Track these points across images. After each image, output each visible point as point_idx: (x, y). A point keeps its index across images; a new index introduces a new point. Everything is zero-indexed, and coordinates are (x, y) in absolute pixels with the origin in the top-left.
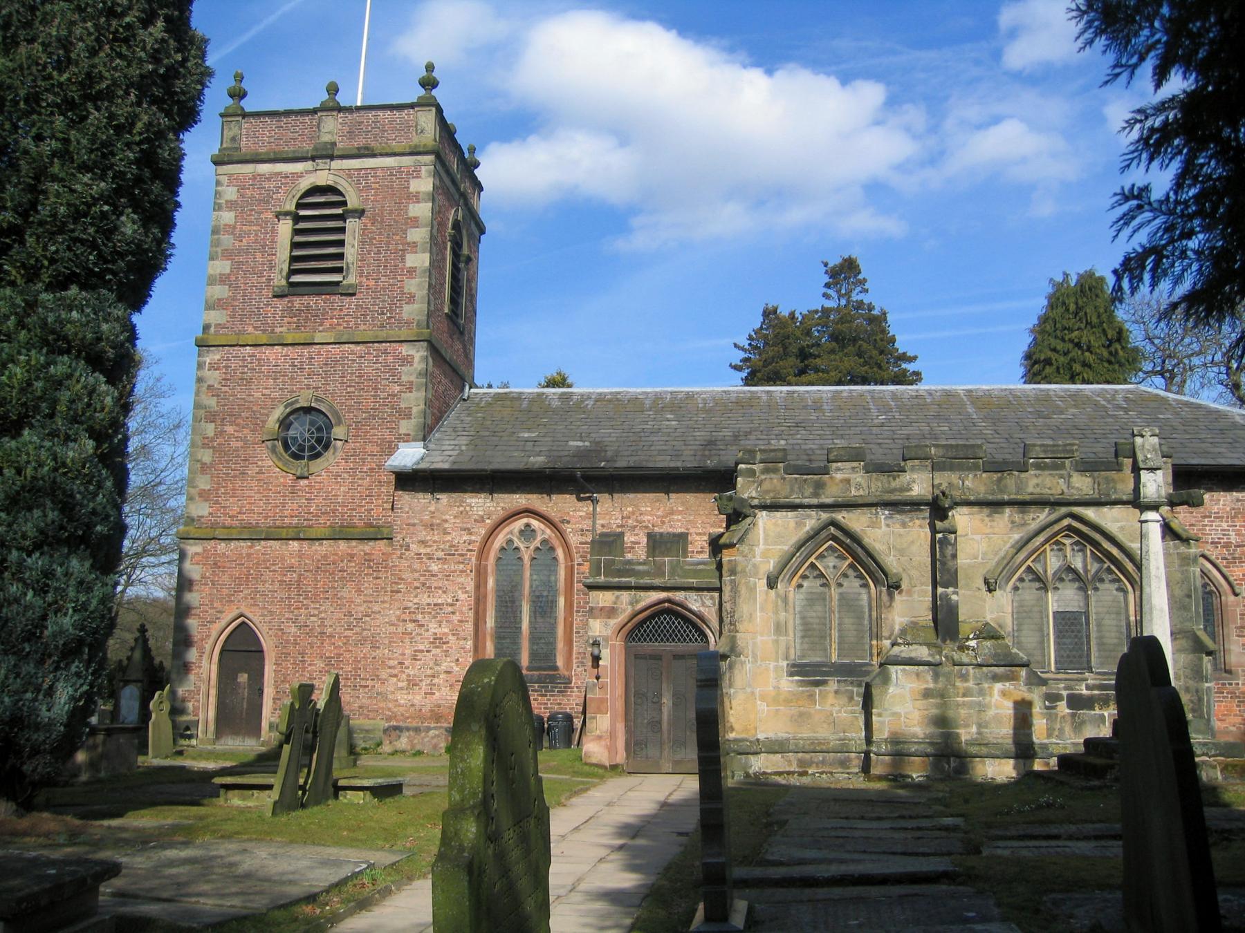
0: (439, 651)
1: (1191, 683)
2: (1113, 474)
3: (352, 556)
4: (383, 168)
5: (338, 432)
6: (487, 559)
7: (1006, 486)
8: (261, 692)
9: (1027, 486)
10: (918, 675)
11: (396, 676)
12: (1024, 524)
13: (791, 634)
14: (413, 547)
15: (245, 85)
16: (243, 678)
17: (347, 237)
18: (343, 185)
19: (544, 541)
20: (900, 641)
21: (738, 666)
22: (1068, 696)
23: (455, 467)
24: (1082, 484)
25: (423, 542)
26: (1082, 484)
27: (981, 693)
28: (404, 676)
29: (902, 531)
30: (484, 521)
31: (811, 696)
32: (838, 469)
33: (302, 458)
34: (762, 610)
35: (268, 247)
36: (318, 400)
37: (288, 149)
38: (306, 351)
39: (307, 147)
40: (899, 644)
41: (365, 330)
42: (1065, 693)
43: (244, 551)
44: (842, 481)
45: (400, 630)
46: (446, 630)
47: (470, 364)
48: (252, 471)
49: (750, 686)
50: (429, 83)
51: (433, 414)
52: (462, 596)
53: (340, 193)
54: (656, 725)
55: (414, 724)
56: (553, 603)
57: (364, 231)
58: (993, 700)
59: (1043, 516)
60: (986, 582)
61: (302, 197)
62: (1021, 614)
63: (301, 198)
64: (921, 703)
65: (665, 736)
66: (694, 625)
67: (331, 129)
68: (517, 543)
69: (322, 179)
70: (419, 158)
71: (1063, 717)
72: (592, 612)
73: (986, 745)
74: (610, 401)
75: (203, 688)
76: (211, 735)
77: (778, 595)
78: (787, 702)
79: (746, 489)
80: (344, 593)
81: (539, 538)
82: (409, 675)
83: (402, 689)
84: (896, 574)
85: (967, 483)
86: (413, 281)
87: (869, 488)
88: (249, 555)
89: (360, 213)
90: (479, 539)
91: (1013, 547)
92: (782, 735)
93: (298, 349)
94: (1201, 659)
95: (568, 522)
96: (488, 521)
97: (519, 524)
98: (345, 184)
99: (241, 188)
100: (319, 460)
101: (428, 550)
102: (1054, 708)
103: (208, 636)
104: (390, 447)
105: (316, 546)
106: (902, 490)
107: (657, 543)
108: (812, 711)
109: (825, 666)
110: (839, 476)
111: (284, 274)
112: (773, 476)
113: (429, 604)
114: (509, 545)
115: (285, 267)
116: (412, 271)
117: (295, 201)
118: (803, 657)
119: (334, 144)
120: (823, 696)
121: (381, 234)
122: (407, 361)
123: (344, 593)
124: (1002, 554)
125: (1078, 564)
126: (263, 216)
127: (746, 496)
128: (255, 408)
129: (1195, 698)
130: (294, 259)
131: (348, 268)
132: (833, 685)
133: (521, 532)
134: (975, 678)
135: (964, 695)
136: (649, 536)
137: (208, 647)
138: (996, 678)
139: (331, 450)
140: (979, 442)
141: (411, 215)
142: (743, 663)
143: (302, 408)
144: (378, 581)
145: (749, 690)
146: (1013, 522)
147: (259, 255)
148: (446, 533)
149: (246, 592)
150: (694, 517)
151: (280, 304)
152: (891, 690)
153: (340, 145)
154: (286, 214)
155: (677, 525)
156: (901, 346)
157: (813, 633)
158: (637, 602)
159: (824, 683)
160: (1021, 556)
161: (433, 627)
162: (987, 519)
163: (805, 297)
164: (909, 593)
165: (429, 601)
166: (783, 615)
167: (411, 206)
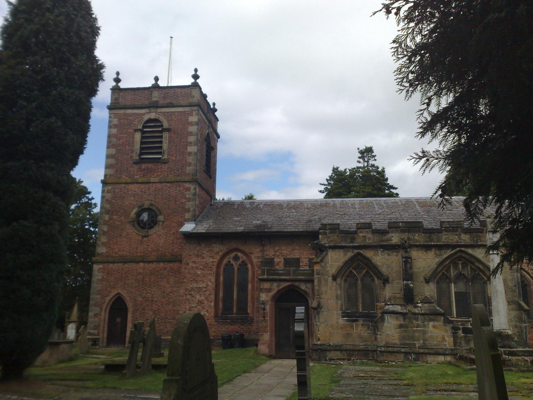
0: (200, 307)
1: (518, 324)
2: (480, 234)
3: (165, 268)
4: (178, 112)
5: (161, 218)
12: (441, 255)
14: (190, 264)
15: (120, 77)
17: (164, 140)
18: (162, 118)
19: (243, 262)
21: (321, 313)
23: (207, 232)
24: (465, 238)
26: (465, 238)
27: (424, 326)
29: (388, 257)
31: (352, 326)
32: (361, 232)
33: (145, 228)
36: (151, 205)
37: (138, 104)
38: (147, 186)
39: (146, 102)
40: (388, 305)
41: (171, 178)
42: (461, 327)
44: (363, 237)
45: (184, 298)
48: (124, 234)
49: (326, 321)
50: (196, 77)
51: (199, 211)
52: (210, 284)
57: (170, 137)
58: (430, 329)
59: (449, 252)
60: (425, 279)
61: (144, 124)
62: (440, 292)
64: (398, 330)
67: (156, 96)
68: (232, 262)
69: (153, 116)
70: (192, 108)
71: (461, 337)
72: (261, 290)
73: (427, 348)
74: (270, 205)
75: (102, 324)
77: (337, 284)
78: (342, 328)
79: (323, 240)
81: (241, 260)
86: (190, 158)
89: (168, 130)
91: (436, 264)
92: (340, 343)
94: (521, 314)
95: (253, 253)
96: (221, 253)
97: (233, 255)
99: (120, 119)
100: (152, 229)
101: (196, 265)
105: (151, 265)
107: (288, 262)
111: (138, 154)
113: (196, 288)
114: (229, 264)
115: (138, 151)
116: (190, 154)
117: (142, 125)
119: (157, 102)
122: (188, 189)
126: (129, 131)
127: (323, 243)
128: (126, 208)
129: (520, 331)
130: (142, 149)
131: (164, 153)
132: (361, 322)
135: (417, 327)
136: (285, 259)
137: (104, 307)
138: (431, 320)
139: (157, 225)
140: (421, 220)
142: (323, 312)
143: (145, 208)
145: (326, 323)
146: (436, 254)
147: (127, 147)
148: (203, 258)
150: (303, 254)
151: (136, 167)
152: (385, 324)
153: (161, 102)
155: (296, 254)
156: (390, 182)
157: (350, 299)
158: (280, 286)
161: (198, 297)
162: (424, 252)
163: (349, 163)
165: (197, 286)
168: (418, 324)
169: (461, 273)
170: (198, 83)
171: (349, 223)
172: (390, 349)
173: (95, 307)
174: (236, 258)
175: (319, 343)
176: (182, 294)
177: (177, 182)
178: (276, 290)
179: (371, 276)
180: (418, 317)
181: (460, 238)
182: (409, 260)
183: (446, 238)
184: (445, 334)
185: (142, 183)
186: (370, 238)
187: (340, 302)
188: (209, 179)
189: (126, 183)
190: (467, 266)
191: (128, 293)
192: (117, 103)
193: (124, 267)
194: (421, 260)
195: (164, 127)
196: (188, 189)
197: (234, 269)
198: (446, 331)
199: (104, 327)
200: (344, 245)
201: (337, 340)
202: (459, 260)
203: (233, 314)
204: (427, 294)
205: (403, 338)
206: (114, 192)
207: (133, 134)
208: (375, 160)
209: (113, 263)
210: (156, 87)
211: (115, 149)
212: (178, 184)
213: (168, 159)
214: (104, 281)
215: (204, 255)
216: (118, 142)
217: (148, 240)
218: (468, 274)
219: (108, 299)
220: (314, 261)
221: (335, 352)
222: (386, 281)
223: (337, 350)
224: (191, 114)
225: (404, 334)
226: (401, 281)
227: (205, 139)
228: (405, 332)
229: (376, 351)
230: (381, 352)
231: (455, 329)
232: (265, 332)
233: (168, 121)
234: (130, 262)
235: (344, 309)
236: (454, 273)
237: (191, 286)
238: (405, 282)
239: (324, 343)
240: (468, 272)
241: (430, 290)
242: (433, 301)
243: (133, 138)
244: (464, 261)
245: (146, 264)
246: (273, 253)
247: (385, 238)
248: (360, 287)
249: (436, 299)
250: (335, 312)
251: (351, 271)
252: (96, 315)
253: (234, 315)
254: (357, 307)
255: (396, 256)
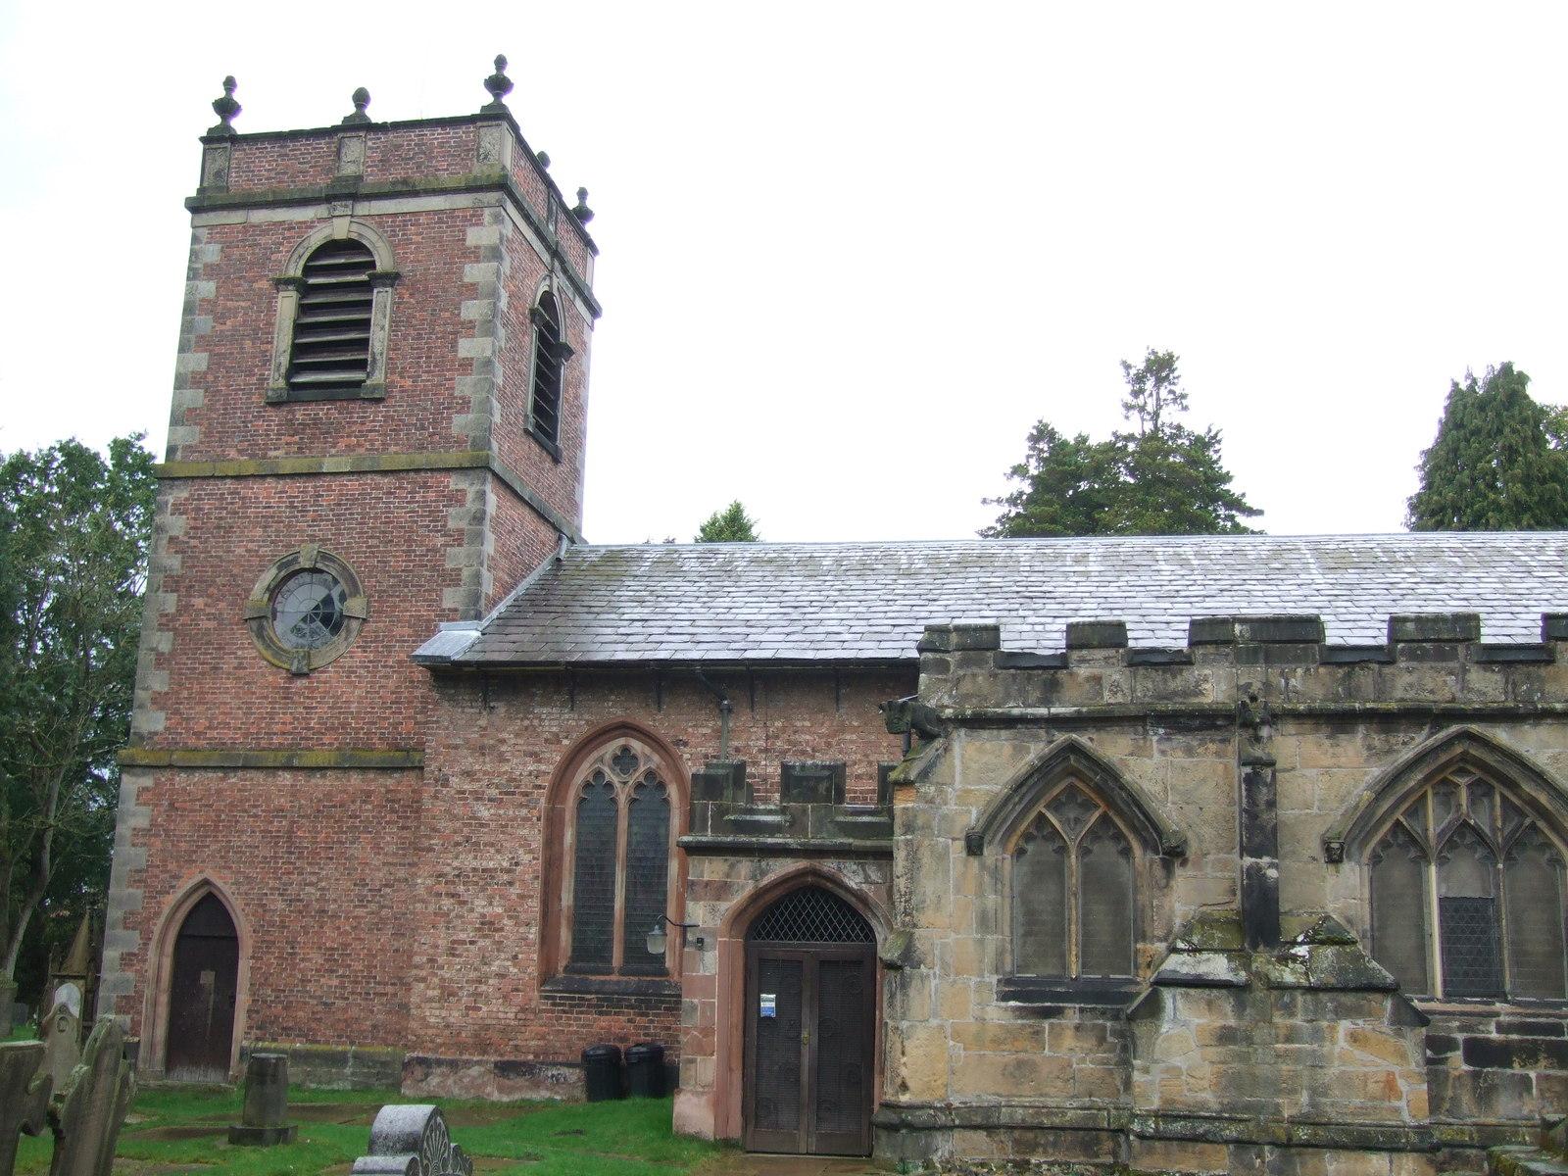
0: (488, 942)
2: (1543, 671)
3: (369, 794)
4: (428, 213)
6: (564, 800)
7: (1358, 688)
8: (232, 1000)
9: (1393, 687)
10: (1209, 1003)
11: (424, 980)
12: (1390, 751)
13: (1007, 930)
14: (454, 781)
16: (207, 978)
17: (375, 316)
18: (371, 238)
19: (650, 774)
20: (1181, 945)
21: (916, 983)
22: (1467, 1041)
25: (468, 774)
27: (1317, 1035)
28: (436, 980)
29: (1187, 761)
30: (559, 742)
31: (1037, 1033)
32: (1082, 661)
34: (958, 891)
35: (263, 333)
36: (325, 557)
39: (322, 182)
41: (396, 456)
42: (1460, 1037)
43: (213, 786)
44: (1088, 679)
45: (431, 908)
46: (500, 910)
47: (573, 506)
48: (228, 664)
49: (935, 1015)
50: (498, 85)
52: (526, 858)
53: (369, 253)
54: (792, 1072)
55: (449, 1057)
56: (662, 870)
57: (397, 305)
58: (1337, 1050)
59: (1421, 740)
60: (1328, 850)
61: (312, 258)
62: (1381, 898)
63: (310, 259)
64: (1214, 1052)
65: (805, 1093)
66: (850, 908)
67: (355, 156)
68: (611, 776)
69: (341, 229)
70: (480, 196)
71: (1459, 1077)
74: (771, 561)
76: (159, 1067)
77: (983, 867)
78: (997, 1042)
79: (935, 695)
80: (355, 850)
81: (642, 769)
82: (443, 979)
83: (431, 1000)
84: (1175, 833)
85: (1293, 682)
87: (1133, 690)
88: (219, 792)
89: (392, 279)
90: (551, 768)
92: (990, 1099)
93: (300, 484)
95: (686, 744)
96: (566, 742)
97: (612, 747)
98: (374, 237)
99: (227, 246)
101: (476, 786)
102: (1444, 1061)
103: (157, 914)
104: (427, 627)
106: (1186, 694)
108: (1037, 1058)
109: (1060, 984)
110: (1083, 671)
111: (283, 370)
112: (976, 670)
113: (474, 870)
114: (597, 784)
115: (285, 360)
117: (302, 263)
118: (1020, 968)
119: (359, 178)
120: (1056, 1034)
121: (422, 310)
122: (456, 498)
123: (355, 850)
124: (1352, 801)
125: (1481, 820)
126: (256, 286)
127: (932, 703)
128: (235, 571)
130: (297, 349)
132: (1072, 1016)
133: (616, 759)
134: (1306, 1010)
135: (1288, 1039)
136: (785, 767)
137: (157, 930)
138: (1341, 1012)
141: (466, 280)
142: (924, 978)
144: (405, 833)
145: (934, 1022)
146: (1370, 748)
147: (248, 343)
148: (502, 758)
149: (213, 847)
150: (857, 745)
151: (275, 416)
152: (1165, 1028)
154: (288, 282)
157: (1038, 927)
158: (763, 873)
159: (1056, 1012)
160: (1385, 806)
161: (479, 904)
162: (1327, 742)
163: (1099, 417)
164: (1198, 866)
165: (475, 864)
166: (992, 899)
167: (467, 268)
168: (1292, 1029)
169: (1465, 824)
170: (504, 107)
171: (1035, 633)
172: (1177, 1127)
173: (126, 928)
174: (625, 760)
175: (905, 1098)
176: (421, 891)
177: (417, 471)
178: (749, 888)
179: (1118, 836)
180: (1293, 999)
181: (1465, 686)
182: (1267, 772)
183: (1409, 684)
184: (1397, 1070)
185: (292, 476)
186: (1119, 687)
187: (992, 940)
188: (548, 464)
189: (238, 478)
190: (1489, 792)
191: (237, 883)
192: (220, 189)
193: (224, 785)
194: (1312, 772)
195: (379, 268)
196: (456, 498)
197: (614, 801)
198: (1403, 1056)
199: (155, 1004)
200: (1016, 711)
201: (975, 1088)
202: (1462, 772)
203: (610, 972)
204: (1334, 908)
205: (1232, 1082)
206: (198, 509)
207: (271, 299)
208: (1185, 408)
209: (190, 769)
210: (357, 125)
211: (205, 355)
212: (420, 478)
213: (389, 387)
214: (157, 835)
215: (504, 748)
216: (219, 327)
217: (312, 690)
218: (1494, 829)
219: (170, 900)
220: (893, 776)
221: (969, 1134)
222: (1174, 855)
223: (976, 1127)
224: (474, 217)
225: (1236, 1066)
226: (1235, 856)
227: (533, 312)
228: (1244, 1058)
229: (1122, 1131)
230: (1141, 1137)
231: (1438, 1046)
232: (702, 1050)
233: (394, 246)
234: (244, 768)
235: (1008, 968)
236: (1437, 824)
237: (456, 864)
238: (1248, 860)
239: (926, 1098)
240: (1493, 820)
241: (1343, 892)
242: (1353, 934)
243: (271, 310)
244: (1479, 774)
245: (301, 777)
246: (762, 743)
247: (1176, 684)
248: (1074, 880)
249: (1367, 927)
250: (975, 979)
251: (1041, 817)
252: (127, 960)
253: (614, 978)
254: (1062, 957)
255: (1218, 754)
